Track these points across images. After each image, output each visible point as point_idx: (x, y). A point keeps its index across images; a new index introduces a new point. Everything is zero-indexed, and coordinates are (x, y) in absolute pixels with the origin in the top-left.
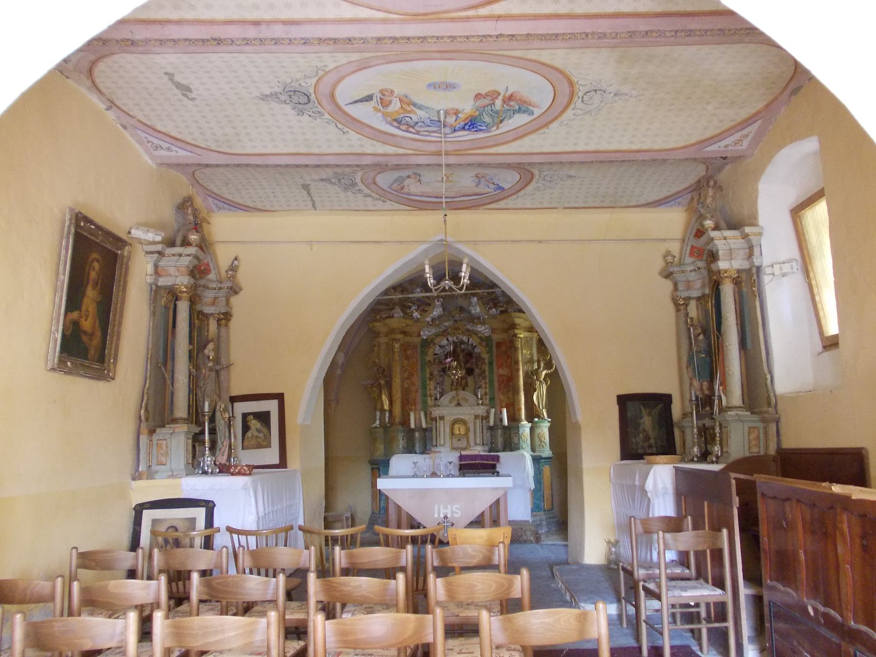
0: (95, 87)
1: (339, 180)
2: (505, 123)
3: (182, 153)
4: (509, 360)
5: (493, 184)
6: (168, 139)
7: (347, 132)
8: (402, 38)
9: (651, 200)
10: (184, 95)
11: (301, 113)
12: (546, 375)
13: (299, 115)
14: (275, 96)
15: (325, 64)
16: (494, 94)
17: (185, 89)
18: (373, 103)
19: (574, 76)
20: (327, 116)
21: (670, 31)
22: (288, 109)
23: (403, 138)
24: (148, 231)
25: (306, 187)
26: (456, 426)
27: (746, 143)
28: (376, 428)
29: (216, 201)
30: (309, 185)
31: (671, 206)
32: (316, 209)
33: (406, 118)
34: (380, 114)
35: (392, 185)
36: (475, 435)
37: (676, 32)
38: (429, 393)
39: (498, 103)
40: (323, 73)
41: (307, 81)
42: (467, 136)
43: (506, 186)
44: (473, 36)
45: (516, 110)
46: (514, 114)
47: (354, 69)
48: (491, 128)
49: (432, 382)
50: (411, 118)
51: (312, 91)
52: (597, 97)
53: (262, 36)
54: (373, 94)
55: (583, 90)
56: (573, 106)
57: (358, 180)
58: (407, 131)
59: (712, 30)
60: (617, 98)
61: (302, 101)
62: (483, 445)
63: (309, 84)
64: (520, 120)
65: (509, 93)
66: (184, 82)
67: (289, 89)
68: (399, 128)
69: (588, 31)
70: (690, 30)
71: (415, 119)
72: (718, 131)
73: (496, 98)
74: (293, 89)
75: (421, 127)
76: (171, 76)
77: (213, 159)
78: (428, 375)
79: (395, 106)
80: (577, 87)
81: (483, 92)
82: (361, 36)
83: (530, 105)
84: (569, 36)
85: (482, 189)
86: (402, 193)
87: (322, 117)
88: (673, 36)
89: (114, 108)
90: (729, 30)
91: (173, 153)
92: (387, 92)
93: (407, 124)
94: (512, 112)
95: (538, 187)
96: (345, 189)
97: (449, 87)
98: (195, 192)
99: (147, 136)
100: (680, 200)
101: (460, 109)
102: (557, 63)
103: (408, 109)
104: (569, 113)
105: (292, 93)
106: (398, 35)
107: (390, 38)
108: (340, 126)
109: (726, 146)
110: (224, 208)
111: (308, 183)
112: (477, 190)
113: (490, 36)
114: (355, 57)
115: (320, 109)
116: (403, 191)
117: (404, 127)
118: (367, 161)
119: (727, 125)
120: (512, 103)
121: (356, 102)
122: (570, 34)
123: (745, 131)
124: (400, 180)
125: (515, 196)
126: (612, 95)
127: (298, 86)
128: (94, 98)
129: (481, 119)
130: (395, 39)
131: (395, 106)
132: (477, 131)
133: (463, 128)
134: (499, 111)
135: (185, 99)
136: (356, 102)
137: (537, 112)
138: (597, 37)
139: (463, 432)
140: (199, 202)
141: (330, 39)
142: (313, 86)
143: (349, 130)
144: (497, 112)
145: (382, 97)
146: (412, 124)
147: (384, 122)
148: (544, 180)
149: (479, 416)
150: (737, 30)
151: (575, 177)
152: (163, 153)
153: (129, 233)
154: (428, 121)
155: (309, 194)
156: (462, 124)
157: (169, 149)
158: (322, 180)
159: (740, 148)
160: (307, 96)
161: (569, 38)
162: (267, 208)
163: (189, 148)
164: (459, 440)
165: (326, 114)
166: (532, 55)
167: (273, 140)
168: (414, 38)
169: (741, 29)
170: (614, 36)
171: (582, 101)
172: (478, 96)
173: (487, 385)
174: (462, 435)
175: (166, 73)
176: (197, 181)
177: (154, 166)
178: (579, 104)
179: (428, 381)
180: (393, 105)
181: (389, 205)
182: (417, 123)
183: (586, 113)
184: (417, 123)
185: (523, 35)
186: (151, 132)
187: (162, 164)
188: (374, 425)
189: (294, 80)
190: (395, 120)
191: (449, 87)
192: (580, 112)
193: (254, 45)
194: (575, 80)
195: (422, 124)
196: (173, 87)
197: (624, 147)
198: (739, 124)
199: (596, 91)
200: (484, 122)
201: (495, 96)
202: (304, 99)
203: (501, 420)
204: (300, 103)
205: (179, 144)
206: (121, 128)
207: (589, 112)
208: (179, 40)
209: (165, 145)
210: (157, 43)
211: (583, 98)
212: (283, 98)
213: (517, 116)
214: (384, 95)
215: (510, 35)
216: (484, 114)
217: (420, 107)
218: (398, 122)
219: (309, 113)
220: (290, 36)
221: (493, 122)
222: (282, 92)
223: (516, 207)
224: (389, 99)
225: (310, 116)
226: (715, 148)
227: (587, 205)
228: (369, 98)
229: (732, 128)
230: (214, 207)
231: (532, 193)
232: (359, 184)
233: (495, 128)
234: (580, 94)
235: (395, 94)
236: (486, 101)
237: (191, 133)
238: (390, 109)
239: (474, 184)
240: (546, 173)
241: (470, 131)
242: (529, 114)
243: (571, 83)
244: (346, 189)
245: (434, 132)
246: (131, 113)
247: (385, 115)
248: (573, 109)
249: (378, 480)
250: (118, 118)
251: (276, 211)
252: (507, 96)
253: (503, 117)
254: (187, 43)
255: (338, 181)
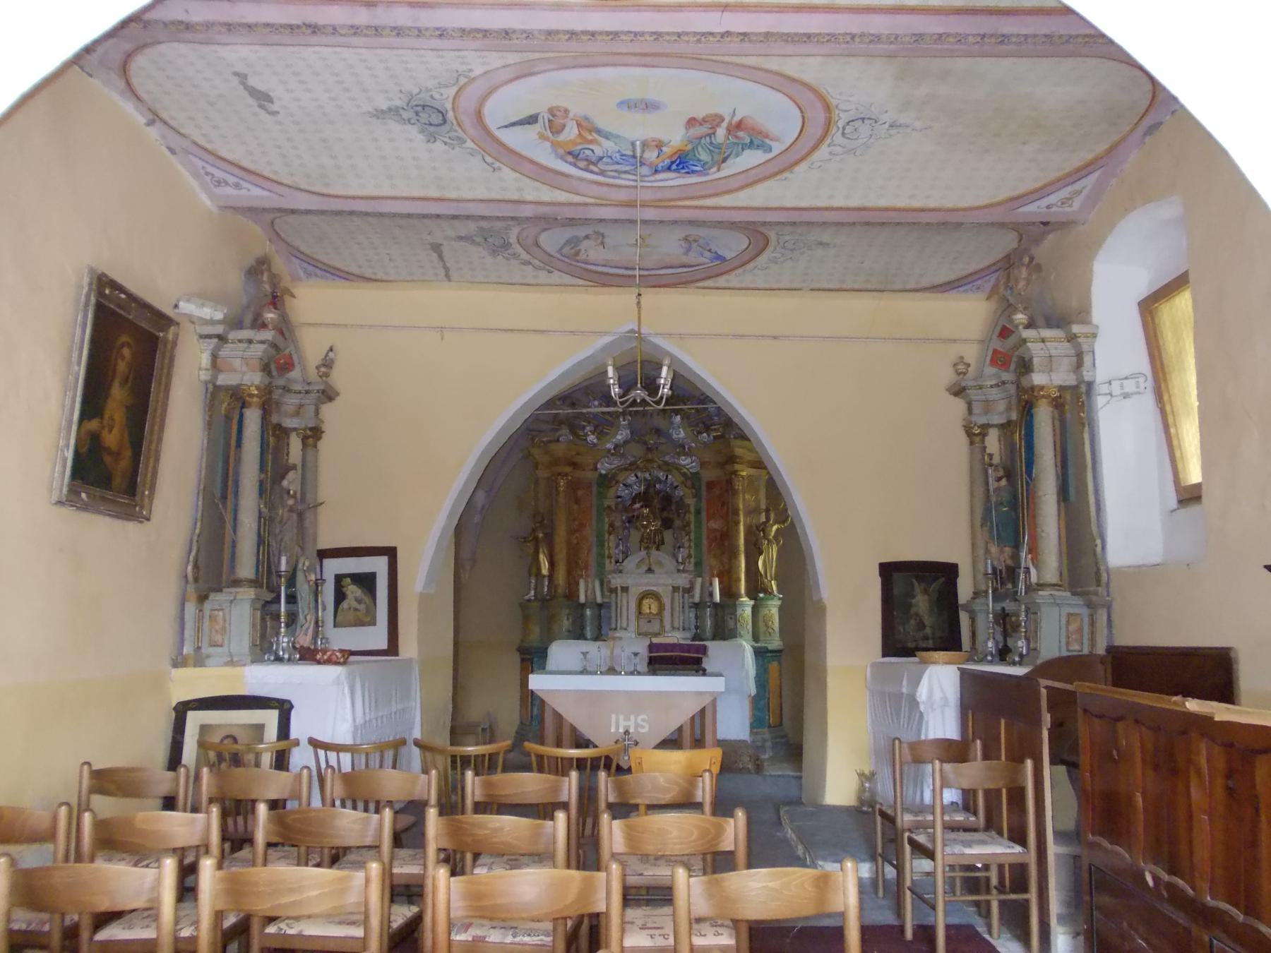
0: (131, 91)
1: (486, 239)
2: (730, 161)
3: (256, 191)
4: (725, 508)
5: (710, 251)
6: (237, 171)
7: (500, 169)
8: (584, 33)
9: (942, 278)
10: (261, 106)
11: (432, 138)
12: (778, 530)
13: (429, 141)
14: (394, 112)
15: (469, 67)
16: (715, 120)
17: (263, 98)
18: (538, 127)
19: (832, 97)
20: (470, 144)
21: (974, 35)
22: (413, 131)
23: (582, 179)
24: (203, 305)
25: (437, 248)
26: (646, 602)
27: (1077, 203)
28: (529, 601)
29: (305, 265)
30: (441, 245)
31: (966, 291)
32: (450, 280)
33: (586, 151)
34: (548, 144)
35: (562, 248)
36: (672, 615)
37: (983, 36)
38: (607, 553)
39: (721, 133)
40: (466, 80)
41: (442, 91)
42: (673, 180)
43: (728, 255)
44: (687, 34)
45: (746, 144)
46: (743, 150)
47: (512, 76)
48: (709, 169)
49: (612, 537)
50: (593, 151)
51: (449, 106)
52: (864, 129)
53: (377, 22)
54: (538, 114)
55: (844, 118)
56: (829, 141)
57: (513, 240)
58: (587, 170)
59: (1035, 36)
60: (893, 132)
61: (435, 121)
62: (684, 630)
63: (445, 96)
64: (750, 159)
65: (737, 119)
66: (262, 87)
67: (415, 103)
68: (575, 165)
69: (854, 31)
70: (1003, 36)
71: (599, 151)
72: (1038, 185)
73: (718, 125)
74: (420, 103)
75: (607, 164)
76: (242, 77)
77: (303, 202)
78: (606, 527)
79: (571, 132)
80: (837, 112)
81: (700, 115)
82: (523, 27)
83: (767, 136)
84: (827, 38)
85: (692, 258)
86: (578, 261)
87: (463, 145)
88: (978, 42)
89: (158, 124)
90: (1061, 36)
91: (244, 192)
92: (560, 111)
93: (587, 160)
94: (740, 146)
95: (775, 257)
96: (494, 251)
97: (649, 106)
98: (273, 248)
99: (206, 165)
100: (979, 282)
101: (666, 141)
102: (807, 78)
103: (590, 137)
104: (824, 150)
105: (419, 109)
106: (578, 27)
107: (567, 32)
108: (489, 159)
109: (1048, 207)
110: (316, 276)
111: (440, 242)
112: (686, 260)
113: (711, 34)
114: (512, 58)
115: (461, 133)
116: (578, 258)
117: (582, 164)
118: (528, 211)
119: (1053, 175)
120: (741, 134)
121: (513, 124)
122: (828, 35)
123: (1077, 186)
124: (574, 242)
125: (740, 271)
126: (887, 125)
127: (429, 99)
128: (129, 107)
129: (695, 155)
130: (572, 34)
131: (571, 132)
132: (688, 173)
133: (669, 169)
134: (722, 144)
135: (262, 113)
136: (513, 124)
137: (777, 148)
138: (868, 40)
139: (654, 610)
140: (280, 264)
141: (478, 31)
142: (451, 99)
143: (501, 165)
144: (719, 147)
145: (551, 118)
146: (594, 159)
147: (553, 155)
148: (784, 247)
149: (678, 588)
150: (1071, 36)
151: (828, 244)
152: (230, 191)
153: (176, 306)
154: (618, 155)
155: (441, 257)
156: (667, 162)
157: (237, 186)
158: (461, 238)
159: (1068, 209)
160: (442, 113)
161: (828, 41)
162: (378, 277)
163: (267, 184)
164: (650, 622)
165: (469, 141)
166: (773, 64)
167: (390, 177)
168: (601, 33)
169: (1077, 36)
170: (892, 40)
171: (843, 134)
172: (692, 122)
173: (692, 544)
174: (654, 615)
175: (236, 74)
176: (278, 235)
177: (215, 210)
178: (838, 138)
179: (607, 536)
180: (567, 129)
181: (557, 277)
182: (601, 158)
183: (846, 152)
184: (601, 158)
185: (760, 33)
186: (210, 158)
187: (226, 207)
188: (527, 597)
189: (423, 89)
190: (570, 153)
191: (649, 106)
192: (839, 150)
193: (366, 35)
194: (833, 102)
195: (609, 160)
196: (245, 94)
197: (901, 203)
198: (1069, 175)
199: (863, 119)
200: (699, 160)
201: (715, 123)
202: (436, 119)
203: (711, 594)
204: (431, 125)
205: (252, 178)
206: (167, 153)
207: (853, 151)
208: (256, 25)
209: (231, 179)
210: (224, 29)
211: (844, 129)
212: (406, 115)
213: (747, 152)
214: (554, 116)
215: (741, 34)
216: (700, 149)
217: (607, 136)
218: (573, 156)
219: (445, 139)
220: (419, 25)
221: (712, 160)
222: (405, 107)
223: (743, 285)
224: (562, 121)
225: (445, 143)
226: (1033, 209)
227: (845, 286)
228: (532, 120)
229: (1059, 180)
230: (301, 273)
231: (765, 266)
232: (513, 246)
233: (715, 169)
234: (840, 124)
235: (571, 115)
236: (704, 130)
237: (269, 163)
238: (562, 137)
239: (682, 251)
240: (787, 238)
241: (679, 172)
242: (765, 151)
243: (828, 108)
244: (494, 253)
245: (625, 172)
246: (182, 131)
247: (555, 145)
248: (829, 146)
249: (531, 676)
250: (163, 137)
251: (391, 281)
252: (733, 122)
253: (726, 154)
254: (269, 29)
255: (483, 240)
